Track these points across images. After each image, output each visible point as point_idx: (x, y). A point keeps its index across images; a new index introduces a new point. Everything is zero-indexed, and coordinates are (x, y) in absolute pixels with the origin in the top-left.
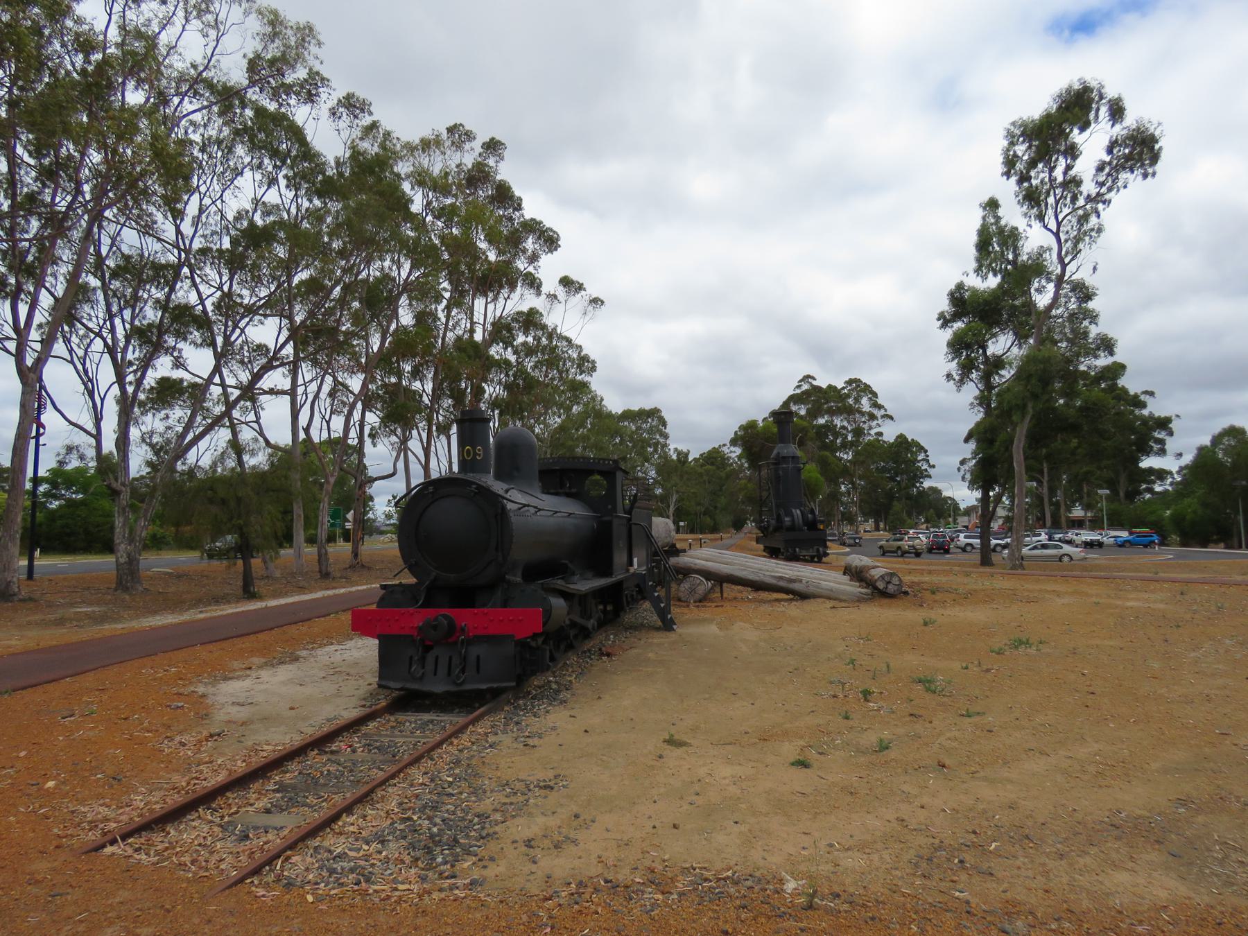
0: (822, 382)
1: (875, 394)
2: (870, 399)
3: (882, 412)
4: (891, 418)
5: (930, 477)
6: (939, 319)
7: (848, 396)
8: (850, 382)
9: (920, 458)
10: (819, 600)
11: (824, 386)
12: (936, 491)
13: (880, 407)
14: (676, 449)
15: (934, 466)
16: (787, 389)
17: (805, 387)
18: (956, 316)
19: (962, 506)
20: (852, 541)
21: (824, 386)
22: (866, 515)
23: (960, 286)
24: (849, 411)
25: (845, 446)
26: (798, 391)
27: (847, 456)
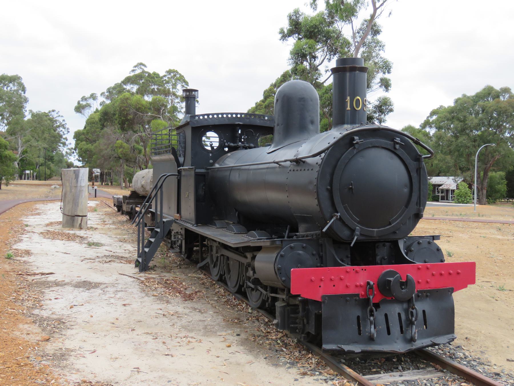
0: (150, 69)
2: (183, 86)
6: (280, 33)
8: (169, 72)
10: (76, 280)
11: (151, 72)
14: (31, 111)
16: (125, 71)
17: (138, 71)
18: (291, 33)
19: (149, 188)
21: (452, 105)
23: (296, 12)
26: (132, 74)
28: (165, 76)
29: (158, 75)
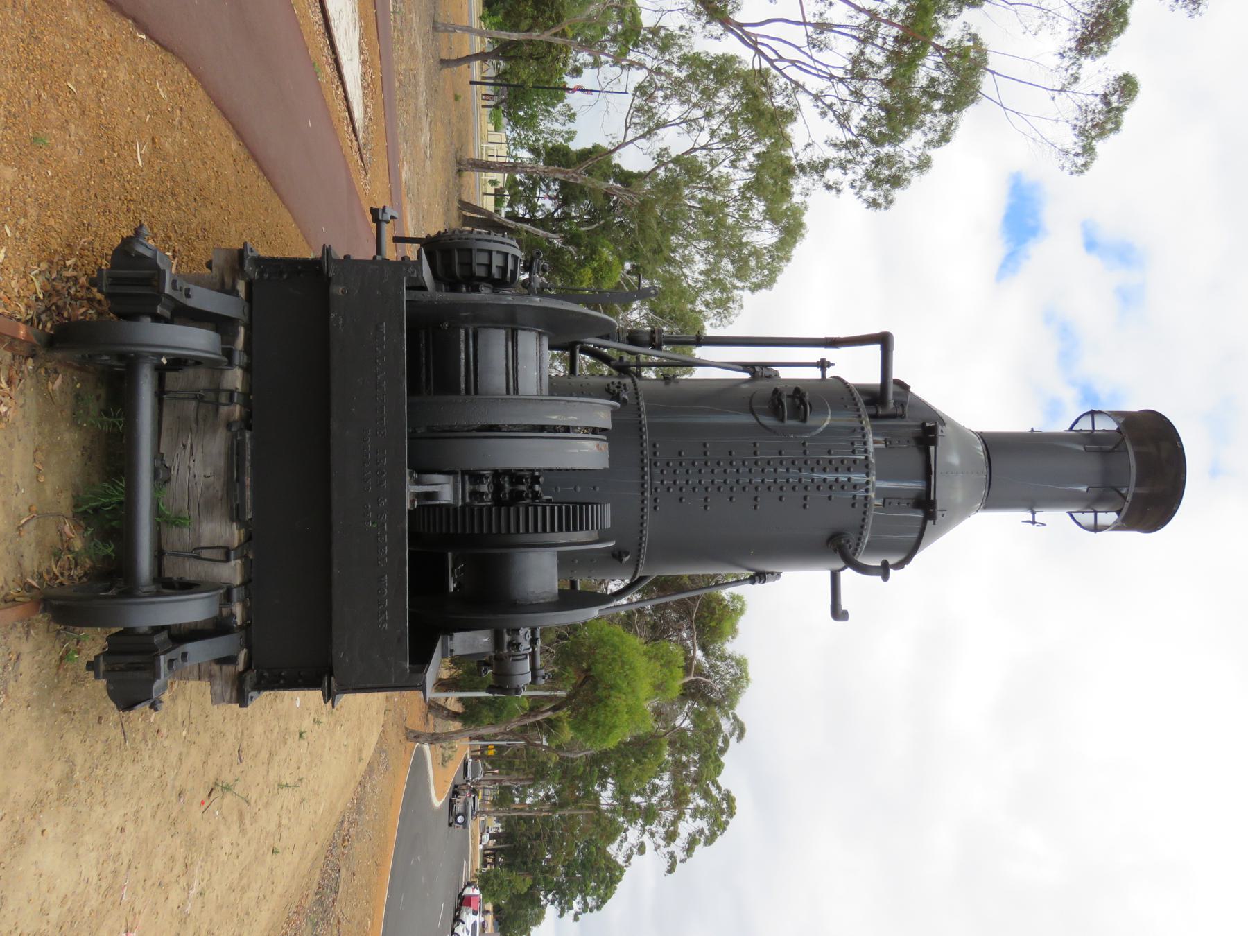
1: (710, 841)
2: (701, 832)
3: (680, 855)
4: (671, 870)
5: (561, 915)
7: (707, 795)
8: (729, 798)
9: (589, 899)
12: (538, 918)
13: (689, 849)
15: (576, 919)
20: (459, 808)
22: (508, 823)
24: (678, 799)
25: (622, 793)
27: (606, 797)
28: (719, 788)
29: (719, 773)
